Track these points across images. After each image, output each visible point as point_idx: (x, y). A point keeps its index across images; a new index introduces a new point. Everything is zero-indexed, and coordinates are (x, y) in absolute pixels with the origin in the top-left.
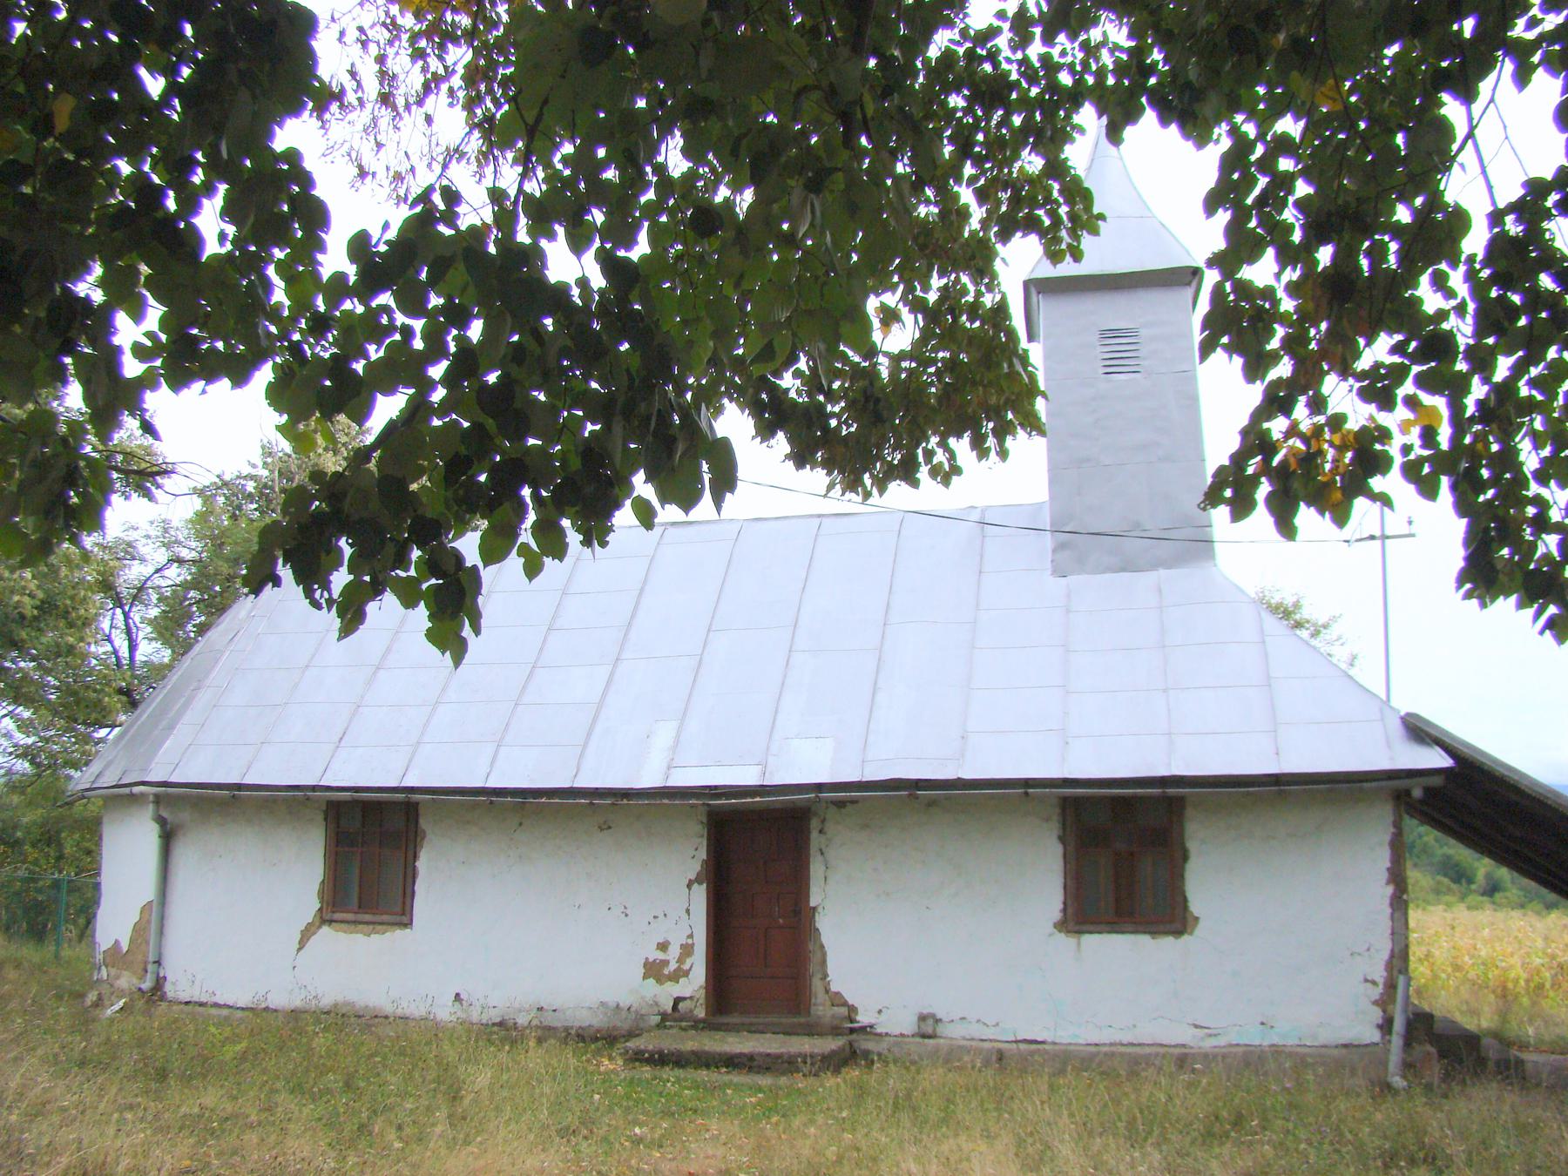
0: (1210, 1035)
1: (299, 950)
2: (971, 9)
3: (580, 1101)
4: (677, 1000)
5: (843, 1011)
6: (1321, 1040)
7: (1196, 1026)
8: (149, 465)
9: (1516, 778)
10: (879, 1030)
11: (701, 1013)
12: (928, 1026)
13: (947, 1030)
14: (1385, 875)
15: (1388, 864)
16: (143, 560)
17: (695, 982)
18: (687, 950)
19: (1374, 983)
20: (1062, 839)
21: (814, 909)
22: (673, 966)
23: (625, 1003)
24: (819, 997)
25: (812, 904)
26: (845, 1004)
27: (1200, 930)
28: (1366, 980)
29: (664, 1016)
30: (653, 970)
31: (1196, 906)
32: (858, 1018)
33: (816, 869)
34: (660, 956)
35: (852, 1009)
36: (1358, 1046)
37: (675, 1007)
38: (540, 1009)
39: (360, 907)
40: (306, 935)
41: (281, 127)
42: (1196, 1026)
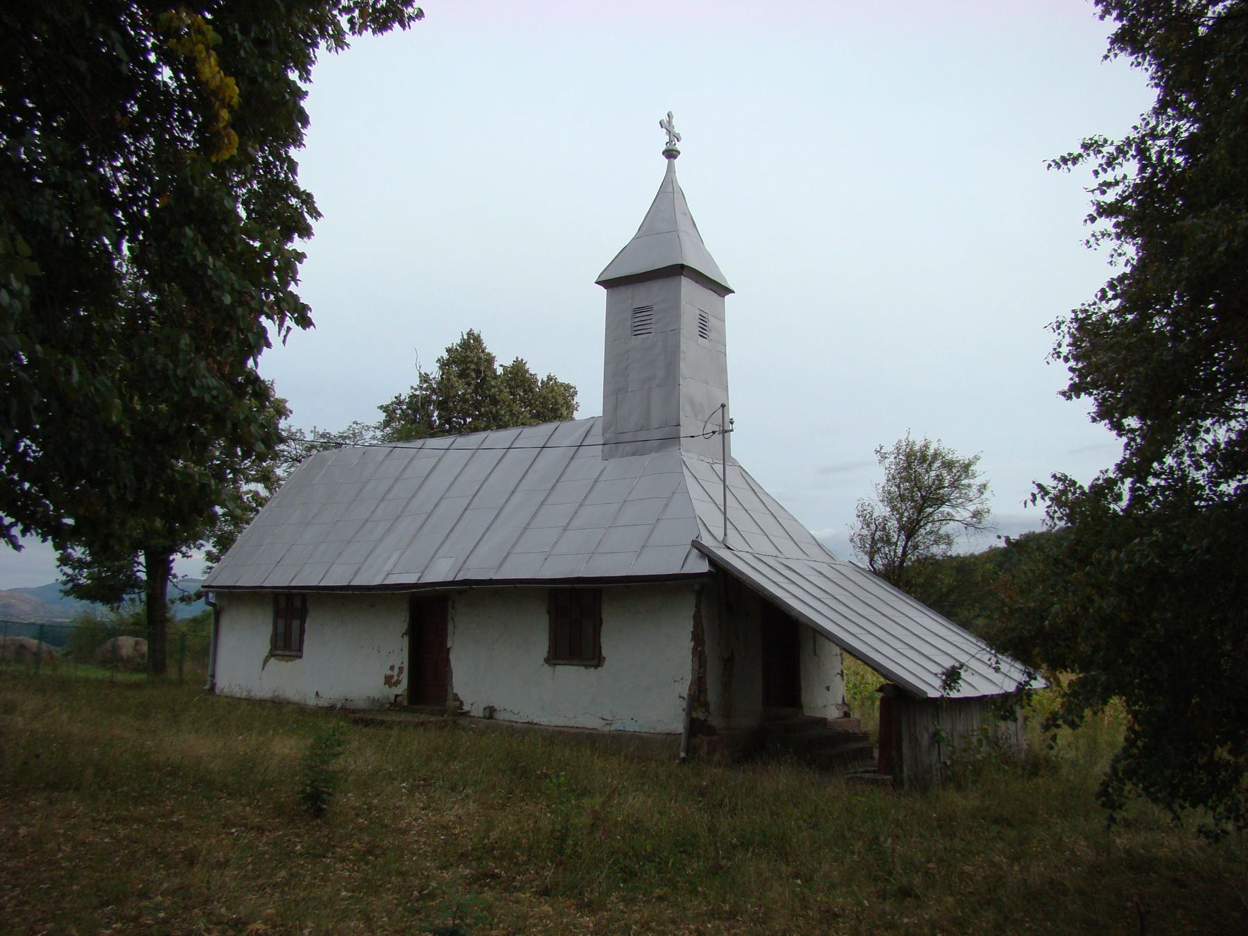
0: (608, 724)
1: (263, 669)
2: (342, 1)
3: (732, 915)
4: (397, 696)
5: (457, 703)
6: (658, 730)
7: (603, 719)
8: (799, 554)
9: (744, 578)
10: (472, 714)
11: (405, 703)
12: (491, 712)
13: (500, 716)
14: (690, 636)
15: (692, 629)
16: (959, 691)
17: (402, 688)
18: (401, 669)
19: (684, 699)
20: (549, 612)
21: (449, 649)
22: (395, 678)
23: (376, 698)
24: (450, 697)
25: (448, 646)
26: (459, 700)
27: (606, 664)
28: (680, 697)
29: (391, 704)
30: (389, 681)
31: (604, 652)
32: (464, 708)
33: (450, 628)
34: (390, 673)
35: (462, 703)
36: (675, 734)
37: (395, 699)
38: (347, 700)
39: (285, 647)
40: (265, 662)
41: (298, 142)
42: (603, 719)
